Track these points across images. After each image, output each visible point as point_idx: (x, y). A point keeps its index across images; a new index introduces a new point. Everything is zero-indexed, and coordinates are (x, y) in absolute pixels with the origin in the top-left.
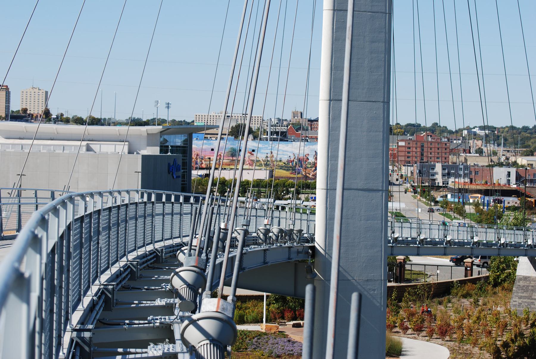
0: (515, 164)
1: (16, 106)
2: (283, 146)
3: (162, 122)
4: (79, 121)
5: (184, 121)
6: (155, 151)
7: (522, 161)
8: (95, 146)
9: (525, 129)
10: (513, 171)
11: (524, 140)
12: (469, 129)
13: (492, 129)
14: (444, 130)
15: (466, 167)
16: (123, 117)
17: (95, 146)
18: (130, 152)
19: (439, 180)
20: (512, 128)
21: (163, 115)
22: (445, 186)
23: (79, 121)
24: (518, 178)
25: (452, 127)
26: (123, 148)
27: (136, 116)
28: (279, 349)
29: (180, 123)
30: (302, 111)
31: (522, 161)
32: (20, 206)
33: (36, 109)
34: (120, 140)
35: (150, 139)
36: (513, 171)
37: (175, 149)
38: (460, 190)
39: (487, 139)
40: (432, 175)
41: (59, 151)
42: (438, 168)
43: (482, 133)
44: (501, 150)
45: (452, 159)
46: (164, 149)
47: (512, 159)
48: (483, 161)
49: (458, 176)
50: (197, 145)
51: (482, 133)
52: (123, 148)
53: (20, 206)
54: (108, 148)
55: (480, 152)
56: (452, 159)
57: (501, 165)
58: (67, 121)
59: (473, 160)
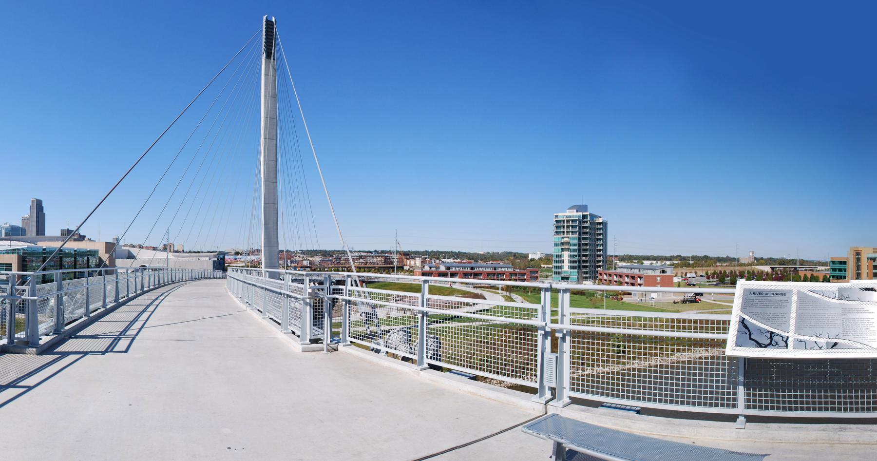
0: (309, 260)
1: (176, 249)
2: (249, 257)
3: (216, 252)
4: (195, 252)
5: (452, 251)
6: (216, 259)
7: (311, 259)
8: (200, 259)
9: (311, 250)
10: (308, 261)
11: (311, 253)
12: (296, 251)
13: (303, 251)
14: (290, 251)
15: (296, 261)
16: (206, 251)
17: (200, 259)
18: (209, 260)
19: (289, 264)
20: (308, 250)
21: (217, 250)
22: (291, 266)
23: (195, 252)
24: (310, 263)
25: (292, 251)
26: (207, 259)
27: (209, 250)
28: (368, 330)
29: (221, 252)
30: (872, 248)
31: (311, 259)
32: (136, 278)
33: (180, 250)
34: (207, 257)
35: (214, 256)
36: (308, 261)
37: (221, 259)
38: (295, 267)
39: (301, 253)
40: (597, 262)
41: (191, 260)
42: (289, 261)
43: (300, 252)
44: (305, 256)
45: (292, 259)
46: (218, 259)
47: (308, 258)
48: (301, 259)
49: (294, 263)
50: (226, 257)
51: (300, 252)
52: (207, 259)
53: (136, 278)
54: (203, 259)
55: (299, 257)
56: (292, 259)
57: (305, 260)
58: (192, 252)
59: (298, 259)
